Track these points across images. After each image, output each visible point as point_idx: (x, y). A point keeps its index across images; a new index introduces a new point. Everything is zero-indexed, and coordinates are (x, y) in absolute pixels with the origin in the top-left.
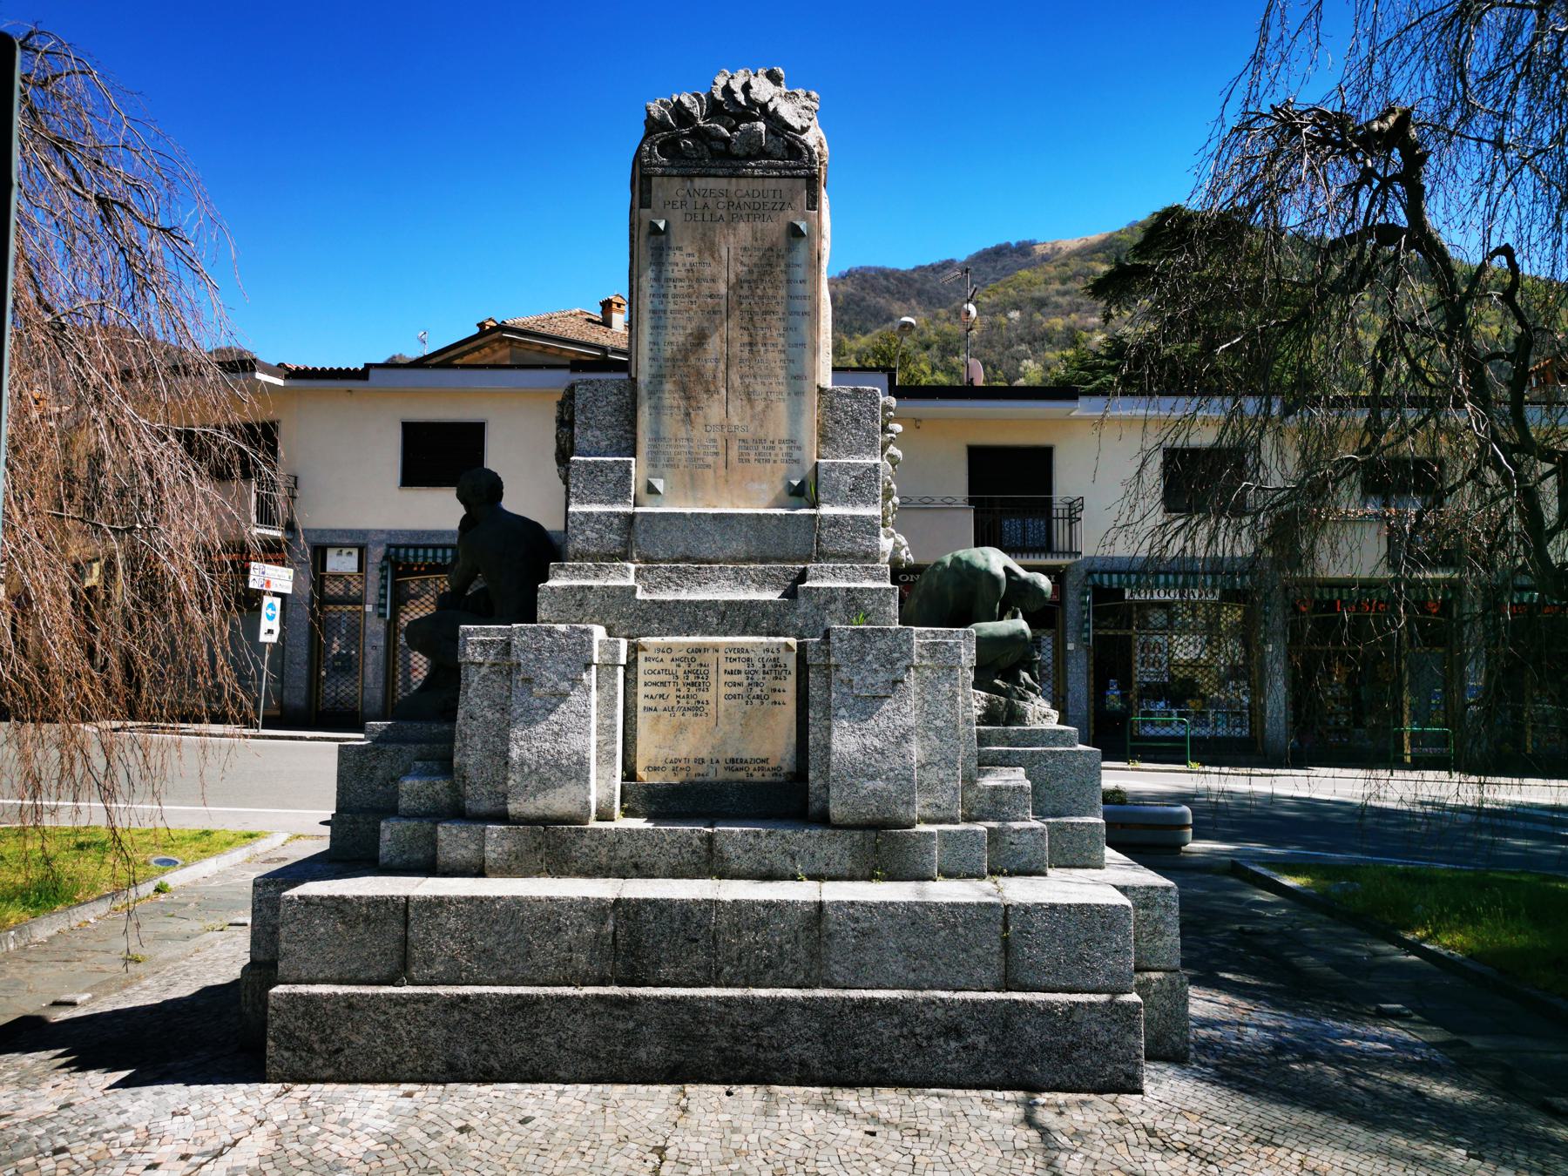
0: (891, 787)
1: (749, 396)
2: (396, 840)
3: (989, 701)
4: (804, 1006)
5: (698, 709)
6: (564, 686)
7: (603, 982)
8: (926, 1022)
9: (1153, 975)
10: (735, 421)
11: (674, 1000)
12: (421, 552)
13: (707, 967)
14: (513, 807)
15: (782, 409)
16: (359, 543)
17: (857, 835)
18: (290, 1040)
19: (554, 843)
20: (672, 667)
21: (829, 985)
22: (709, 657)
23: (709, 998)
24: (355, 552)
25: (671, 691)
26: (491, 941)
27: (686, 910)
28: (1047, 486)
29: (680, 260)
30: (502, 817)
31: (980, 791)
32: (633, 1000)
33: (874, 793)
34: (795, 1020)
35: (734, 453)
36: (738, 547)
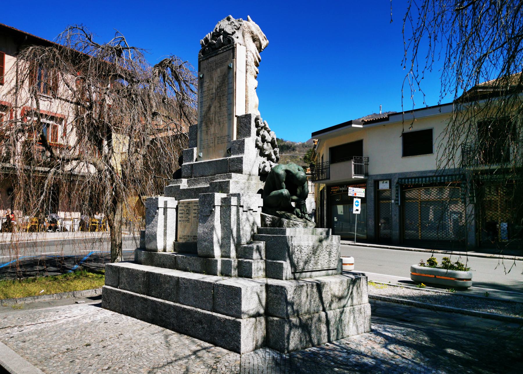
0: (209, 245)
3: (272, 218)
7: (144, 294)
8: (195, 318)
9: (275, 319)
12: (410, 180)
16: (388, 178)
17: (202, 259)
20: (184, 208)
22: (190, 205)
23: (158, 302)
24: (388, 182)
31: (241, 248)
33: (206, 246)
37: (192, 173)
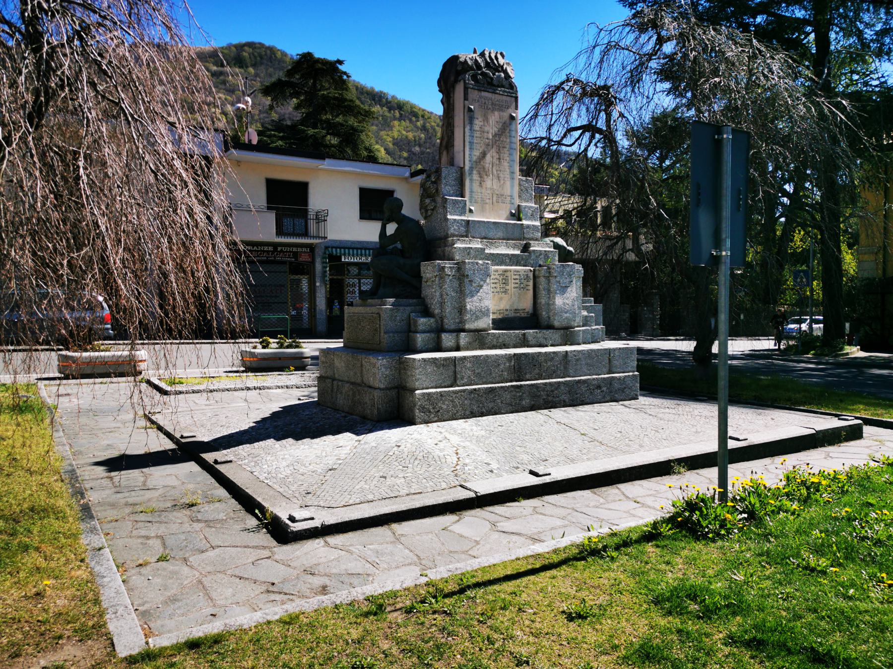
1: (499, 178)
2: (423, 341)
4: (564, 383)
5: (505, 292)
6: (482, 283)
7: (511, 381)
10: (495, 187)
11: (532, 385)
13: (538, 374)
14: (467, 326)
15: (508, 183)
18: (423, 409)
19: (480, 339)
20: (498, 277)
21: (569, 376)
22: (508, 274)
25: (498, 285)
26: (480, 370)
27: (533, 355)
28: (306, 203)
29: (478, 123)
30: (464, 331)
32: (521, 385)
33: (566, 318)
34: (562, 388)
35: (495, 198)
36: (500, 234)
37: (467, 231)
